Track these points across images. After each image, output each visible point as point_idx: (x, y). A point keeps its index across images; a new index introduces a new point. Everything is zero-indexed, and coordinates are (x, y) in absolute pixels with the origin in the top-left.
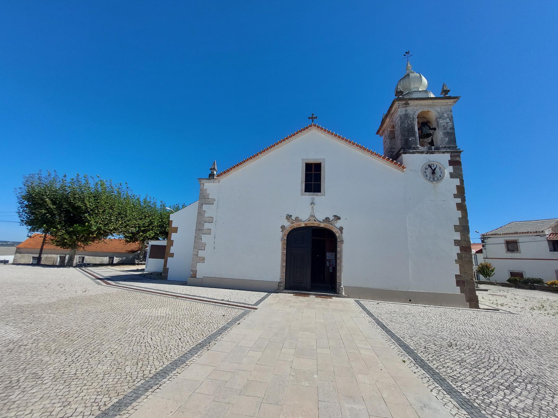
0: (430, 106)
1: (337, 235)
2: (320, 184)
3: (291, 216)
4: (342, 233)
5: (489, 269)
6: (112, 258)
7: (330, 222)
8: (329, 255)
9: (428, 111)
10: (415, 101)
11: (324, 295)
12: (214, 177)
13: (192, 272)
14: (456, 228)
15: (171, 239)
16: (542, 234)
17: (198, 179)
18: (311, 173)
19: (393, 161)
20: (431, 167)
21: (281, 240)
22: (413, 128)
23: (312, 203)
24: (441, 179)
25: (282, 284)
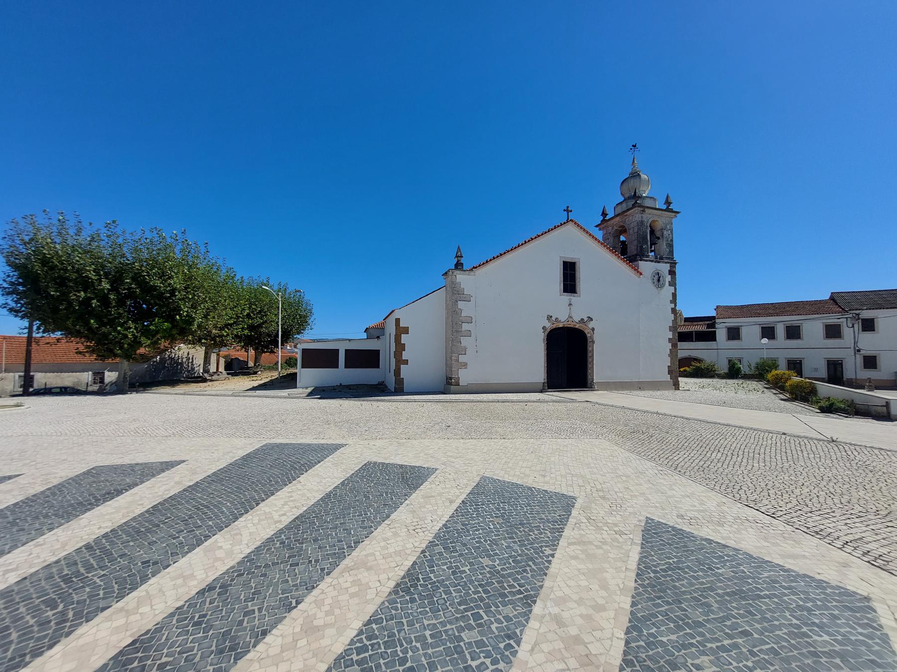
11: (576, 391)
23: (570, 304)
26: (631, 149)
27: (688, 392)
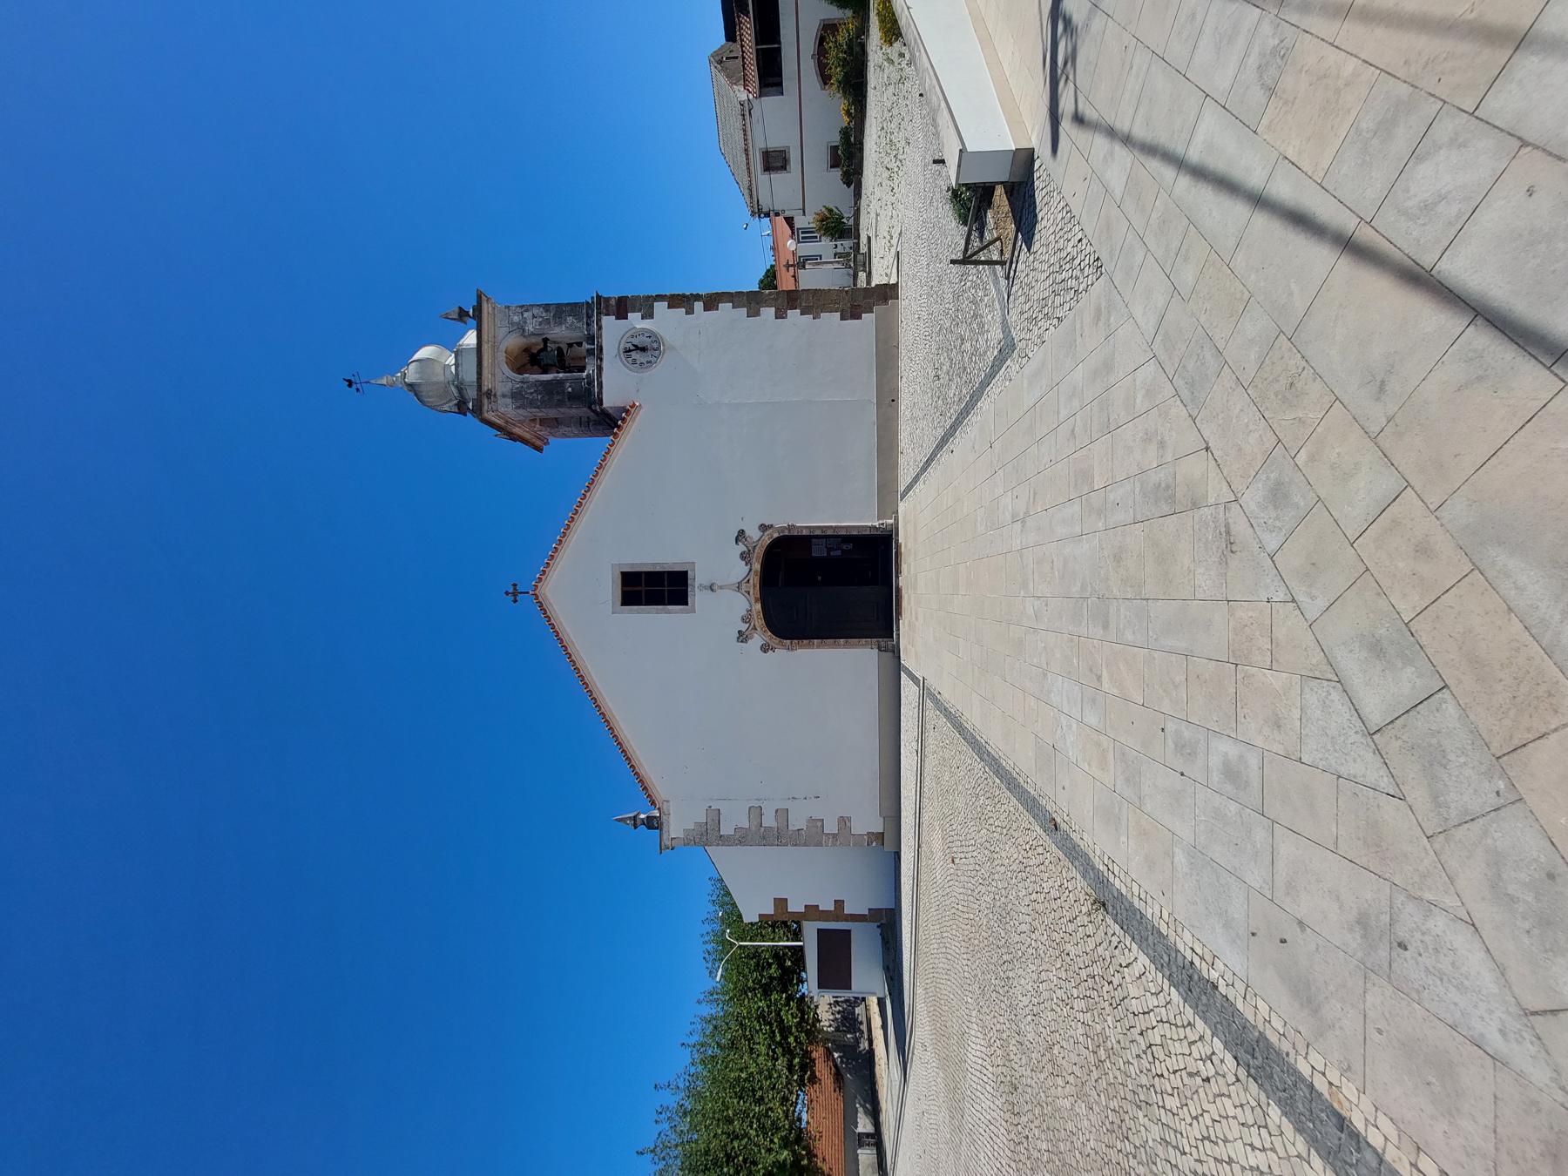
0: (494, 347)
1: (776, 535)
2: (668, 572)
3: (739, 632)
4: (771, 526)
5: (827, 218)
6: (861, 1140)
7: (749, 551)
8: (818, 551)
9: (506, 352)
10: (483, 378)
11: (898, 630)
12: (655, 817)
13: (872, 843)
14: (754, 313)
15: (803, 911)
16: (746, 105)
17: (661, 853)
18: (643, 594)
19: (619, 427)
20: (630, 351)
21: (792, 649)
22: (542, 383)
23: (711, 588)
24: (656, 336)
25: (882, 644)
26: (358, 390)
27: (904, 258)
